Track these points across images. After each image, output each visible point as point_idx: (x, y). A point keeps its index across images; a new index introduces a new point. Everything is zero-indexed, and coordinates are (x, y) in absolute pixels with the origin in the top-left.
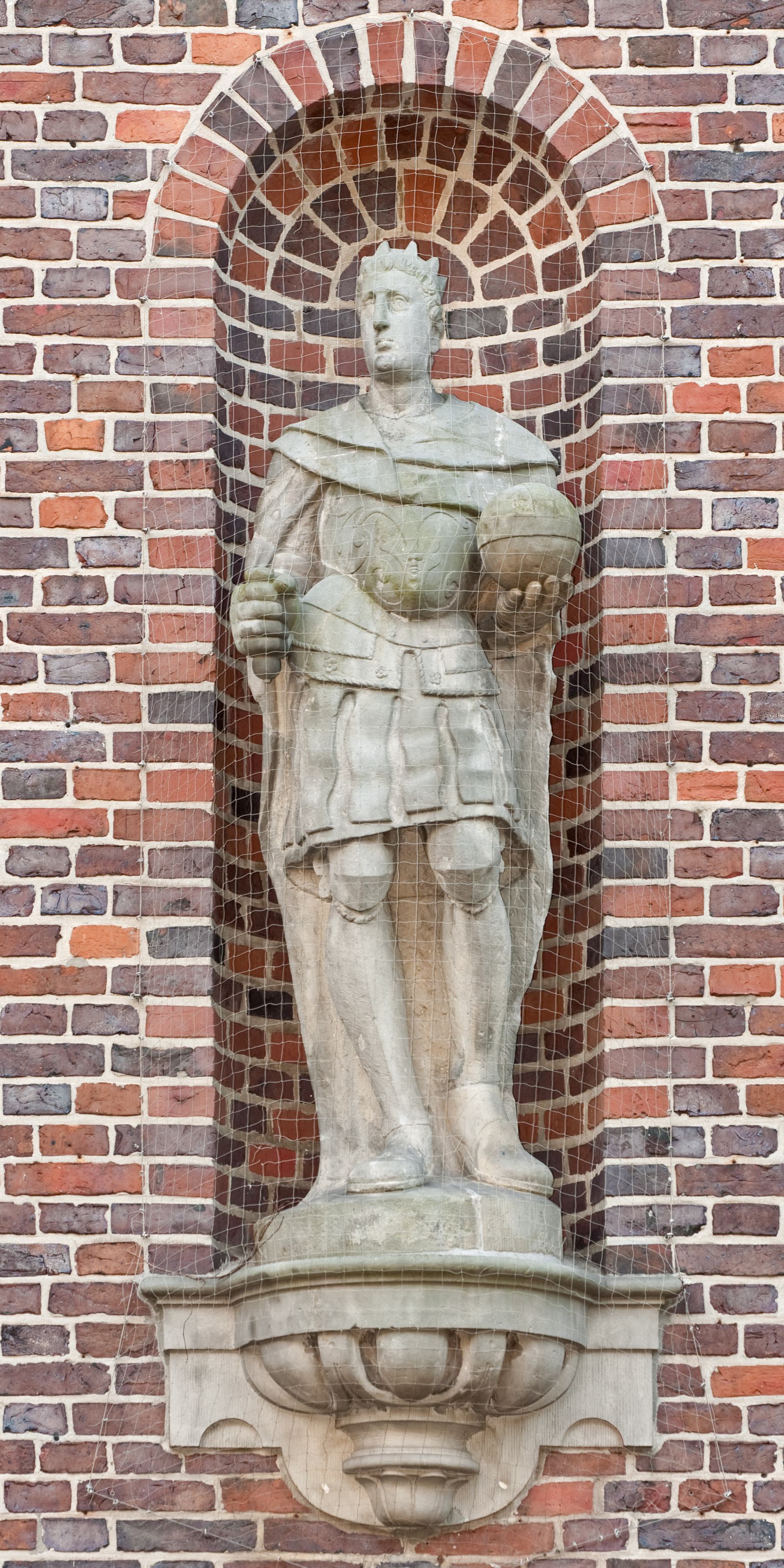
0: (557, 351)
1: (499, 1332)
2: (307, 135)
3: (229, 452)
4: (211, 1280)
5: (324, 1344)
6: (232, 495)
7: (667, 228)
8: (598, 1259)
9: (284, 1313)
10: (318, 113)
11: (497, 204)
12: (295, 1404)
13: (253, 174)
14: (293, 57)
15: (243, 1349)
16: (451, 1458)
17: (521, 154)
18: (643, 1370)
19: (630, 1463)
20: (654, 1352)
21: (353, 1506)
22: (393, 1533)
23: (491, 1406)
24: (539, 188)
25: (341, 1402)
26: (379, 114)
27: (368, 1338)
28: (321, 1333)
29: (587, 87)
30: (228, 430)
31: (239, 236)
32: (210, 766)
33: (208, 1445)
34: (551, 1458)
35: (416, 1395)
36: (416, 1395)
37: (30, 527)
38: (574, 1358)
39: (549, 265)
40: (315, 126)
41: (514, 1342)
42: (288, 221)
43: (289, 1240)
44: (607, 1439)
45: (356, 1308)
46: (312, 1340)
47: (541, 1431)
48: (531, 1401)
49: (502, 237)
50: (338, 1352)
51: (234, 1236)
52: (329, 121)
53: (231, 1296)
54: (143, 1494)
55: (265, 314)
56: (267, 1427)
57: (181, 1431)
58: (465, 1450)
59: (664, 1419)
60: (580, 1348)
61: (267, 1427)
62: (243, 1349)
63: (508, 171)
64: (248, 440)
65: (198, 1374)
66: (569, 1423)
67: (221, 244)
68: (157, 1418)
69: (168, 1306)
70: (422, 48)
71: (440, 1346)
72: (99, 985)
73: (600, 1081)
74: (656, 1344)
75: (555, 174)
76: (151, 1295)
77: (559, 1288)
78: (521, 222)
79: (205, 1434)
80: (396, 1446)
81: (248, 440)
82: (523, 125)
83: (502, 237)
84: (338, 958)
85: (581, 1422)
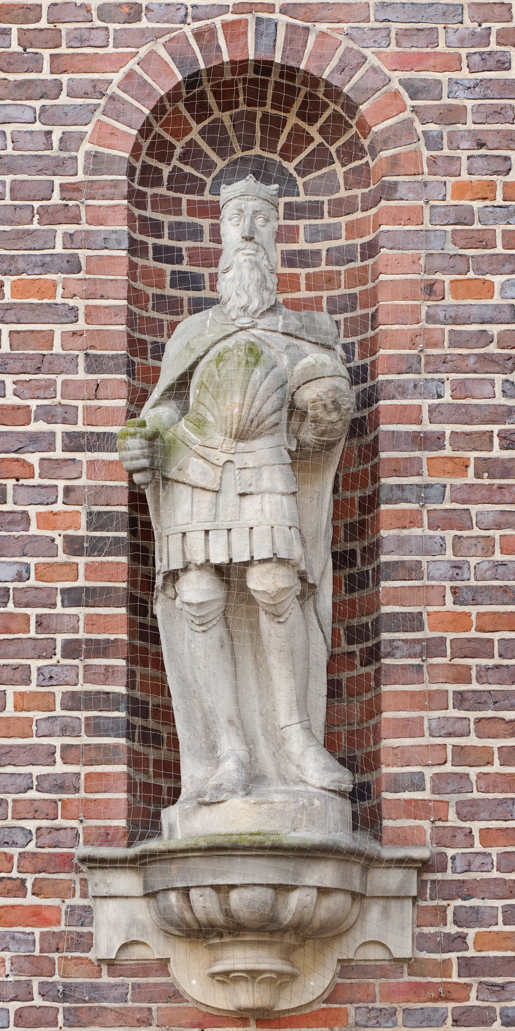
0: (354, 229)
5: (194, 894)
6: (147, 301)
12: (177, 933)
16: (279, 965)
21: (222, 999)
22: (242, 1016)
23: (305, 936)
28: (192, 887)
33: (120, 958)
34: (346, 967)
42: (166, 171)
43: (181, 824)
46: (186, 891)
47: (348, 949)
50: (205, 905)
51: (145, 822)
53: (138, 863)
54: (73, 989)
55: (161, 204)
56: (157, 947)
58: (288, 960)
59: (420, 942)
60: (362, 896)
61: (157, 947)
65: (385, 912)
66: (358, 945)
70: (258, 35)
80: (239, 958)
82: (328, 84)
84: (191, 654)
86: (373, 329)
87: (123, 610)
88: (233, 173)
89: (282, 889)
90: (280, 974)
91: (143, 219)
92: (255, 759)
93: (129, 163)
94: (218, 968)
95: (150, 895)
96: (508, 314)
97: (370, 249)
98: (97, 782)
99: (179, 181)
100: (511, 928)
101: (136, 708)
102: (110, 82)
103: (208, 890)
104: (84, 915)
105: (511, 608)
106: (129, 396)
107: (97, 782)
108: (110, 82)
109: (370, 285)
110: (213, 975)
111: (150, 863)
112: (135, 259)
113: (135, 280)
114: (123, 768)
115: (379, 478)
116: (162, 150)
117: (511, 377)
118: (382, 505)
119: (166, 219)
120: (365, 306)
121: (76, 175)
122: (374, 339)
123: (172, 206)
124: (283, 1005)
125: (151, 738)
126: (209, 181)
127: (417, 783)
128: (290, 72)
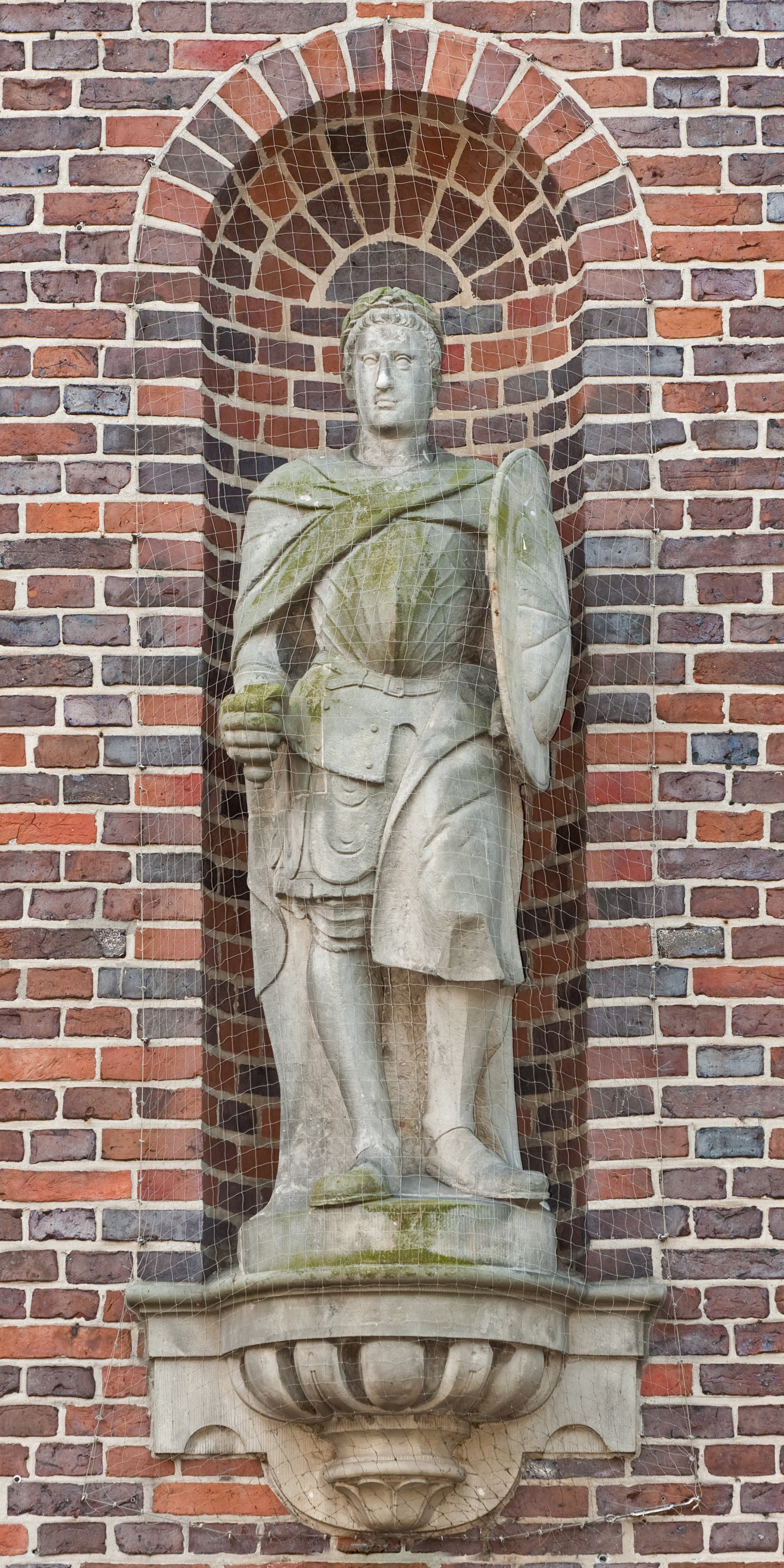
4: (189, 1290)
5: (301, 1353)
8: (579, 1268)
11: (490, 211)
18: (626, 1377)
22: (385, 1537)
23: (477, 1415)
25: (316, 1415)
26: (367, 121)
27: (350, 1349)
29: (585, 99)
30: (216, 434)
31: (222, 240)
32: (199, 770)
35: (399, 1407)
36: (399, 1407)
37: (722, 642)
38: (555, 1365)
39: (536, 268)
41: (436, 1348)
45: (355, 1317)
47: (532, 1434)
48: (513, 1411)
49: (492, 242)
50: (318, 1364)
51: (219, 1243)
56: (253, 1435)
57: (165, 1439)
61: (253, 1435)
67: (207, 252)
68: (144, 1424)
69: (151, 1314)
72: (697, 896)
75: (450, 120)
76: (135, 1304)
78: (511, 227)
83: (492, 242)
85: (565, 1429)
86: (574, 423)
87: (198, 690)
89: (436, 1348)
90: (432, 1480)
91: (226, 410)
92: (393, 1109)
93: (206, 550)
96: (776, 322)
98: (156, 1023)
100: (778, 846)
101: (214, 993)
102: (177, 120)
103: (325, 1346)
104: (139, 1380)
105: (780, 1001)
106: (204, 1069)
107: (156, 1023)
108: (177, 120)
110: (332, 1482)
111: (237, 1305)
112: (215, 550)
114: (198, 1003)
117: (779, 416)
119: (263, 409)
121: (123, 956)
123: (268, 316)
124: (437, 1522)
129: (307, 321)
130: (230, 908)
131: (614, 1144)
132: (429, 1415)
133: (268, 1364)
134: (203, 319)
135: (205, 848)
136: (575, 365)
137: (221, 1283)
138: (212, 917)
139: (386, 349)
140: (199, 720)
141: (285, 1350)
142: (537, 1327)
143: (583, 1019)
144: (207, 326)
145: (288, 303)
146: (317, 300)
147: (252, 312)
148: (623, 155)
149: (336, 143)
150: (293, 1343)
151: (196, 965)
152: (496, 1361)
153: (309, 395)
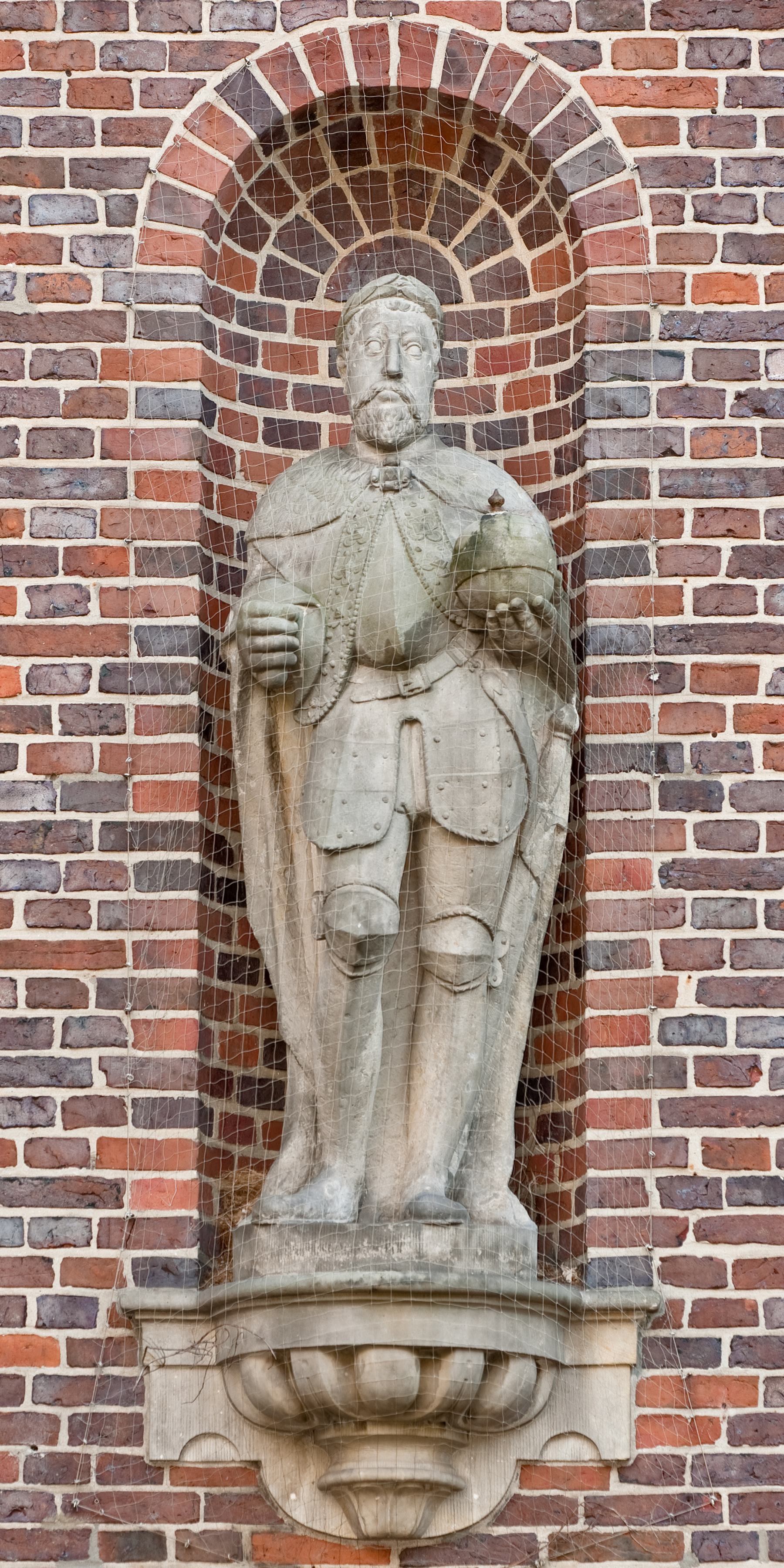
1: (409, 1348)
2: (294, 140)
3: (218, 459)
7: (653, 232)
9: (259, 1328)
10: (304, 117)
13: (239, 177)
14: (323, 50)
15: (220, 1365)
17: (510, 155)
19: (614, 1476)
20: (631, 1366)
21: (333, 1522)
23: (463, 1423)
24: (529, 189)
25: (312, 1425)
27: (346, 1355)
31: (225, 239)
35: (401, 1416)
36: (401, 1416)
40: (301, 129)
41: (495, 1359)
44: (586, 1453)
45: (345, 1325)
47: (528, 1444)
48: (513, 1418)
52: (315, 125)
53: (211, 1313)
62: (220, 1365)
63: (500, 172)
64: (239, 446)
71: (409, 1360)
73: (583, 1093)
74: (632, 1359)
77: (516, 1304)
79: (546, 1445)
81: (239, 446)
88: (363, 266)
94: (331, 1479)
95: (230, 1363)
97: (577, 300)
99: (277, 279)
103: (567, 1362)
109: (575, 282)
111: (229, 1313)
113: (210, 507)
115: (585, 931)
116: (250, 233)
118: (590, 1250)
120: (565, 318)
122: (580, 1230)
125: (229, 969)
126: (324, 281)
127: (634, 1192)
128: (451, 104)
129: (309, 323)
130: (228, 918)
131: (613, 1153)
132: (420, 1422)
133: (258, 1370)
134: (203, 397)
135: (203, 776)
136: (580, 370)
137: (216, 1292)
138: (212, 925)
139: (394, 318)
140: (195, 805)
141: (280, 1360)
142: (537, 1336)
143: (581, 1031)
144: (208, 487)
145: (291, 306)
146: (320, 304)
147: (253, 316)
148: (629, 155)
149: (338, 144)
150: (288, 1351)
151: (193, 817)
152: (487, 1372)
153: (308, 398)
